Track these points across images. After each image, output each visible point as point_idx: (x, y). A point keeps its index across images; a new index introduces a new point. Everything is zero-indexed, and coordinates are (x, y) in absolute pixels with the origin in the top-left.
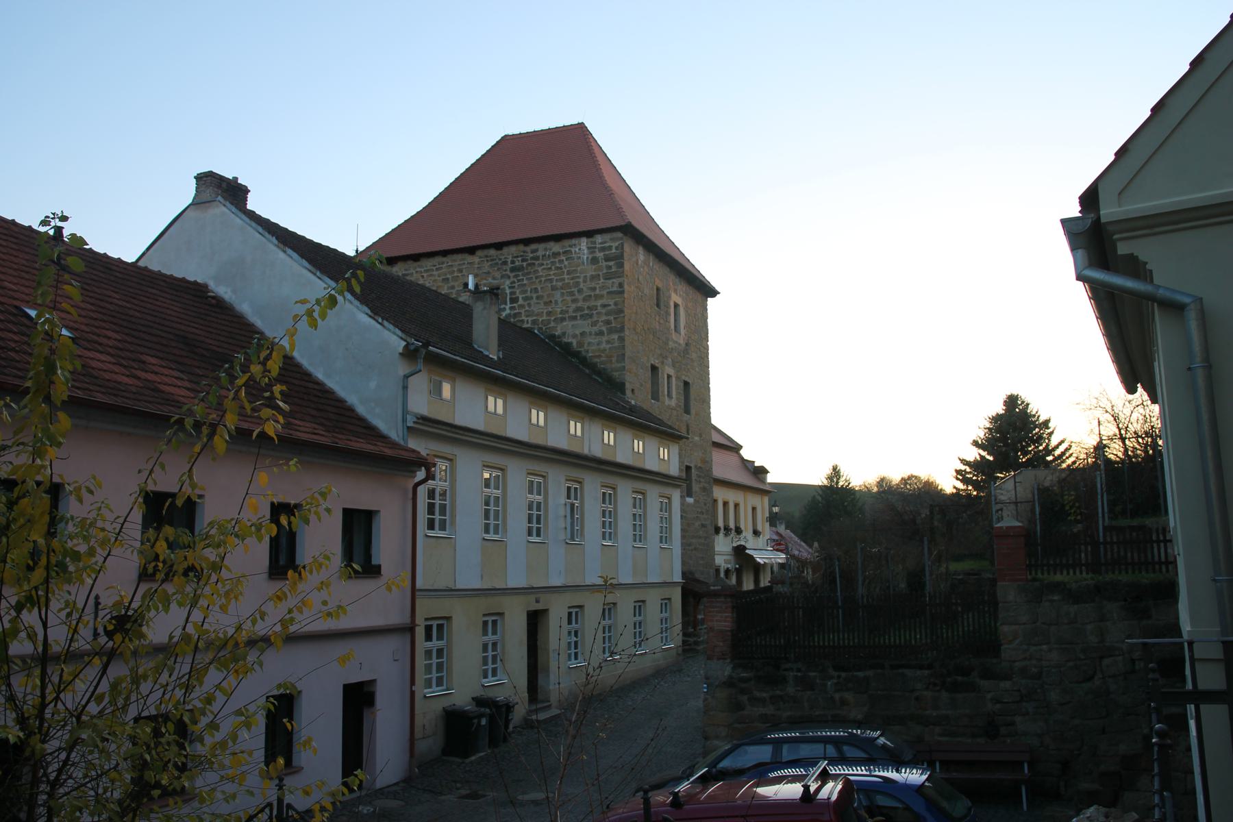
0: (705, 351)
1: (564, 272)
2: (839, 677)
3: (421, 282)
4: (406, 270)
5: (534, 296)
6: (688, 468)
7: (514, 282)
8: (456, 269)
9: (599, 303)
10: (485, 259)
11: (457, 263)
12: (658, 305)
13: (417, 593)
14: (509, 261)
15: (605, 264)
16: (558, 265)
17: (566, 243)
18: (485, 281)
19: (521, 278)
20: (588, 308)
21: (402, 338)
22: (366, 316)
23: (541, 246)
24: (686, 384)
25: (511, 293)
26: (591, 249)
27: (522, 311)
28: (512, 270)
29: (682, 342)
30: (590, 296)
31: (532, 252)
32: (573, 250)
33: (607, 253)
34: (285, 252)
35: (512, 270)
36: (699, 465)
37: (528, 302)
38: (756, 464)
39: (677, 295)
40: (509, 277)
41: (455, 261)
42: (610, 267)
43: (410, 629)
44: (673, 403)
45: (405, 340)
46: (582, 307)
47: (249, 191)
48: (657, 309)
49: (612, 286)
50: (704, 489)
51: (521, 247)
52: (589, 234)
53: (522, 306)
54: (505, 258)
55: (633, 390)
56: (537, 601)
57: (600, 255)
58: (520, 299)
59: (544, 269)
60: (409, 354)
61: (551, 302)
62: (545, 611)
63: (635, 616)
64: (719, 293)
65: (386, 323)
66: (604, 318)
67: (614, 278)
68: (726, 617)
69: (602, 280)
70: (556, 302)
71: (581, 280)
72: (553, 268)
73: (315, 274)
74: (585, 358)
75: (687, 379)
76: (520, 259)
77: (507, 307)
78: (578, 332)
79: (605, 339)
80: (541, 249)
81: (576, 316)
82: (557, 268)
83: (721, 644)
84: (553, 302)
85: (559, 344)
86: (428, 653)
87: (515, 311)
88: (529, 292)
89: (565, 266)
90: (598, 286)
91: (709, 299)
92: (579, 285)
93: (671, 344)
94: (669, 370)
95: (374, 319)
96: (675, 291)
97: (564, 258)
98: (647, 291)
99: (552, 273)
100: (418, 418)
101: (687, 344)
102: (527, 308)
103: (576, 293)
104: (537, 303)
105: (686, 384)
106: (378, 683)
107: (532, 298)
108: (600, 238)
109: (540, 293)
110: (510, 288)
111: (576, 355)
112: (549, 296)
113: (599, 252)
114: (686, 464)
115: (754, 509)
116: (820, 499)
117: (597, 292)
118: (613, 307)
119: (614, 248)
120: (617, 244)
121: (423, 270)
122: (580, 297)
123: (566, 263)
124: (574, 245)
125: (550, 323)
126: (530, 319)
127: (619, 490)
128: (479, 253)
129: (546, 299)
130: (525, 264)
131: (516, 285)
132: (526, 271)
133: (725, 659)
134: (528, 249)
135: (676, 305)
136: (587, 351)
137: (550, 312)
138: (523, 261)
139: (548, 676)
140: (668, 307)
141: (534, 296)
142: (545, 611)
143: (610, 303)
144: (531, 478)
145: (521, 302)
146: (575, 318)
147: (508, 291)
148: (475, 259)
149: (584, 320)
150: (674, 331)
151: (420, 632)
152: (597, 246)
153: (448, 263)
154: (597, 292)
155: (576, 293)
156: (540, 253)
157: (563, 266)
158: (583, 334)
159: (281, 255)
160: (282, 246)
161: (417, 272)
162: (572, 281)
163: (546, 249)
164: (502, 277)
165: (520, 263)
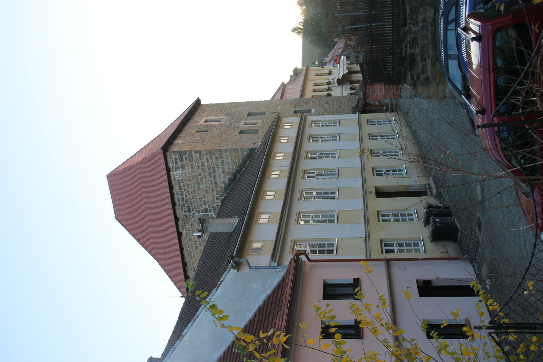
0: (231, 104)
1: (190, 184)
2: (410, 24)
3: (198, 261)
4: (191, 270)
5: (203, 199)
6: (295, 112)
7: (196, 211)
8: (190, 243)
9: (206, 164)
10: (184, 227)
11: (187, 242)
12: (206, 131)
13: (368, 258)
14: (184, 214)
15: (184, 161)
16: (186, 187)
17: (173, 183)
18: (196, 227)
19: (194, 207)
20: (209, 170)
21: (229, 271)
22: (218, 290)
23: (176, 196)
24: (249, 114)
25: (202, 212)
26: (177, 169)
27: (212, 205)
28: (189, 212)
29: (226, 117)
30: (202, 168)
31: (180, 201)
32: (177, 179)
33: (178, 160)
34: (184, 336)
35: (189, 212)
36: (293, 106)
37: (207, 202)
38: (292, 74)
39: (199, 121)
40: (194, 213)
41: (185, 244)
42: (186, 158)
43: (388, 261)
44: (260, 121)
45: (230, 269)
46: (209, 173)
47: (151, 357)
48: (208, 132)
49: (197, 157)
50: (307, 103)
51: (177, 207)
52: (168, 170)
53: (209, 206)
54: (183, 216)
55: (253, 144)
56: (371, 192)
57: (180, 164)
58: (205, 207)
59: (188, 195)
60: (238, 266)
61: (206, 190)
62: (376, 188)
63: (377, 139)
64: (198, 98)
65: (221, 280)
66: (214, 161)
67: (192, 156)
68: (377, 88)
69: (194, 162)
70: (207, 187)
71: (194, 174)
72: (188, 189)
73: (196, 319)
74: (236, 170)
75: (247, 114)
76: (183, 208)
77: (210, 214)
78: (223, 175)
79: (226, 160)
80: (177, 196)
81: (214, 176)
82: (188, 187)
83: (392, 90)
84: (206, 189)
85: (229, 185)
86: (401, 251)
87: (212, 209)
88: (201, 202)
89: (186, 183)
90: (197, 165)
91: (202, 103)
92: (197, 175)
93: (228, 123)
94: (242, 124)
95: (219, 286)
96: (198, 122)
97: (182, 184)
98: (199, 138)
99: (190, 190)
100: (273, 260)
101: (227, 115)
102: (210, 203)
103: (201, 176)
104: (207, 197)
105: (249, 114)
106: (418, 278)
107: (205, 201)
108: (170, 164)
109: (202, 196)
110: (199, 213)
111: (235, 175)
112: (203, 191)
113: (178, 164)
114: (293, 113)
115: (317, 75)
116: (310, 39)
117: (200, 165)
118: (208, 156)
119: (175, 156)
120: (173, 155)
121: (191, 261)
122: (203, 174)
123: (185, 182)
124: (175, 178)
125: (218, 190)
126: (216, 201)
127: (308, 150)
128: (181, 230)
129: (205, 193)
130: (186, 205)
131: (198, 209)
132: (190, 204)
133: (401, 88)
134: (178, 203)
135: (206, 121)
136: (233, 169)
137: (212, 190)
138: (184, 206)
139: (412, 185)
140: (207, 126)
141: (203, 199)
142: (376, 188)
143: (206, 157)
144: (303, 197)
145: (207, 207)
146: (215, 177)
147: (201, 214)
148: (184, 232)
149: (215, 172)
150: (220, 122)
151: (389, 256)
152: (175, 165)
153: (187, 247)
154: (200, 165)
155: (201, 176)
156: (180, 197)
157: (186, 184)
158: (223, 172)
159: (186, 338)
160: (181, 338)
161: (192, 264)
162: (195, 179)
163: (178, 194)
164: (193, 217)
165: (186, 207)
